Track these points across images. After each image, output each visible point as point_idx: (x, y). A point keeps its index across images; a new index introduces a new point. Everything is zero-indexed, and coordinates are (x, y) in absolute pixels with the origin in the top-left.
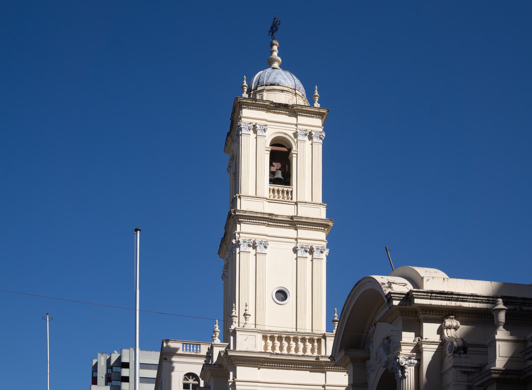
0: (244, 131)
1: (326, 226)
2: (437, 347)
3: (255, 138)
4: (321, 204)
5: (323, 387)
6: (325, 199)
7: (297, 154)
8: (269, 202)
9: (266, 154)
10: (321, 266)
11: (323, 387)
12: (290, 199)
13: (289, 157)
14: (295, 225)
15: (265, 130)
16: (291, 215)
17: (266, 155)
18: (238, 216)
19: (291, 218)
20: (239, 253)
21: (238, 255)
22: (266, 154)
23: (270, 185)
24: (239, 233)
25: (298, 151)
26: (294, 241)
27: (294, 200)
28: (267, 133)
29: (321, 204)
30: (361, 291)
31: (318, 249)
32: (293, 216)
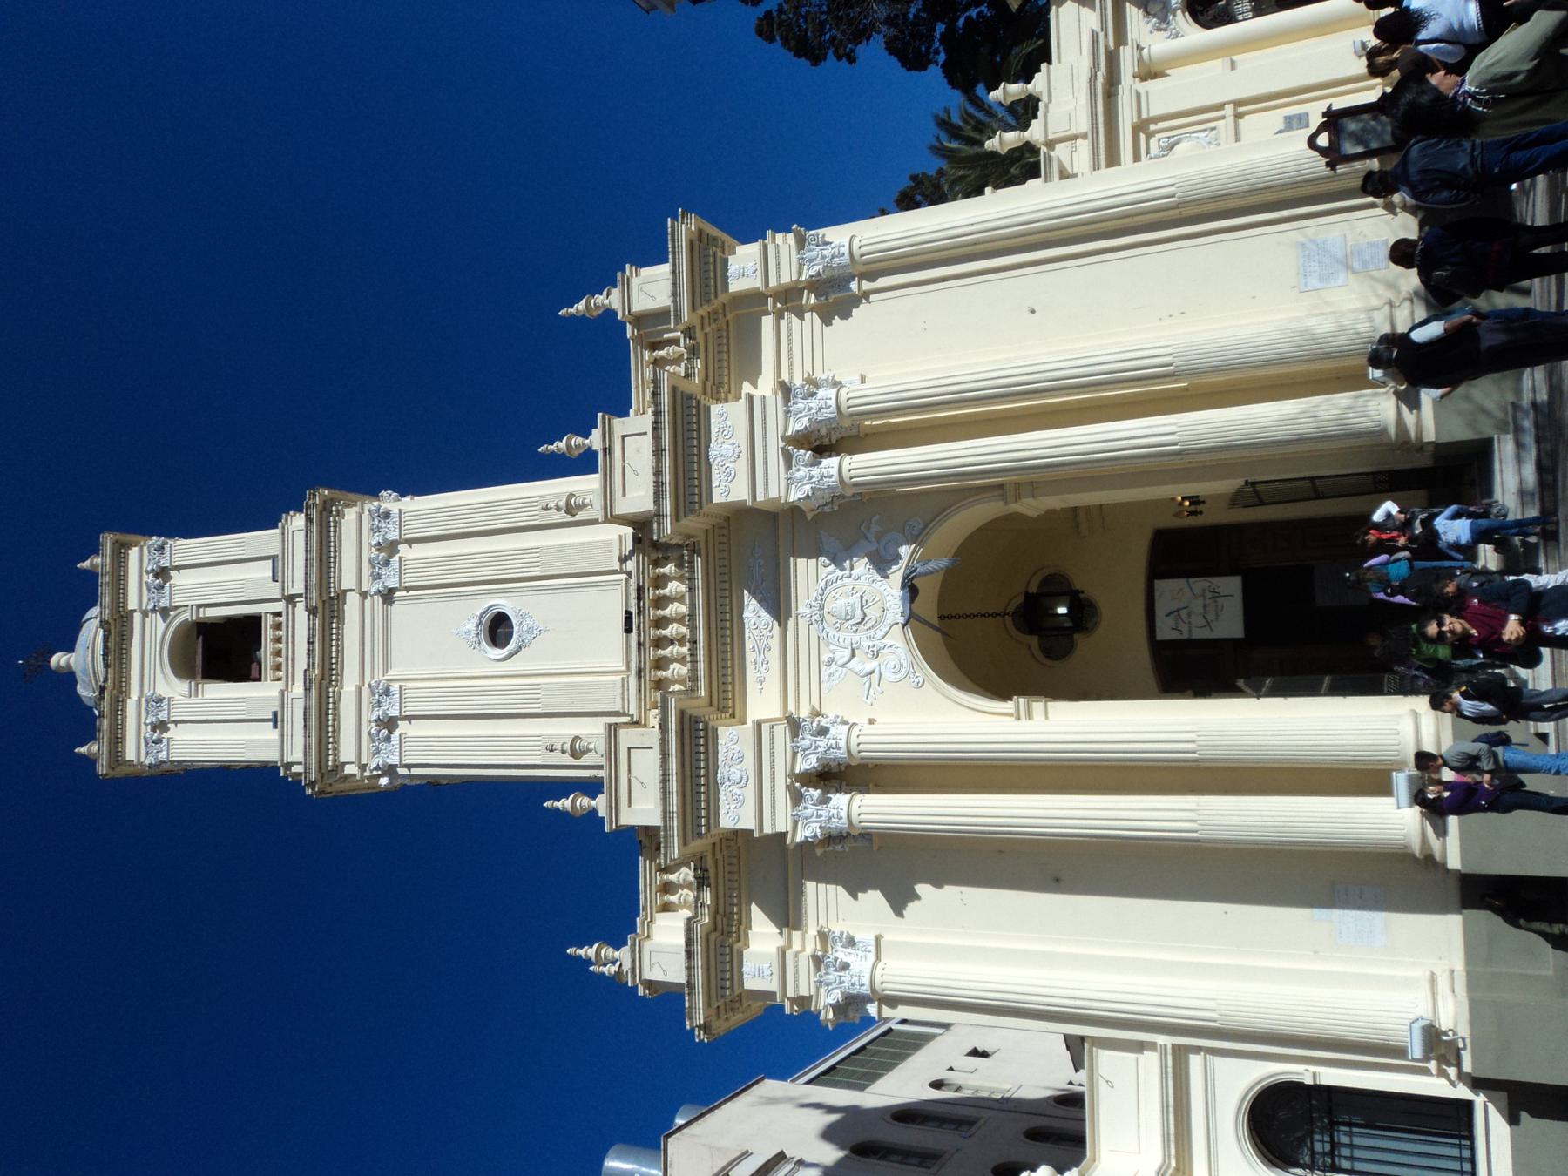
0: (162, 756)
1: (325, 509)
2: (1208, 1056)
3: (176, 725)
4: (283, 534)
5: (148, 617)
6: (267, 519)
7: (199, 606)
8: (293, 683)
9: (203, 695)
10: (184, 549)
11: (148, 617)
12: (281, 619)
13: (222, 622)
14: (332, 598)
15: (160, 700)
16: (306, 613)
17: (206, 696)
18: (324, 771)
19: (315, 615)
20: (409, 767)
21: (415, 771)
22: (203, 695)
23: (266, 680)
24: (363, 767)
25: (190, 603)
26: (368, 602)
27: (279, 606)
28: (162, 690)
29: (283, 534)
30: (1392, 543)
31: (379, 530)
32: (306, 607)
